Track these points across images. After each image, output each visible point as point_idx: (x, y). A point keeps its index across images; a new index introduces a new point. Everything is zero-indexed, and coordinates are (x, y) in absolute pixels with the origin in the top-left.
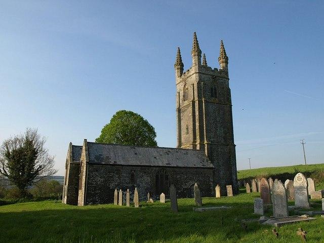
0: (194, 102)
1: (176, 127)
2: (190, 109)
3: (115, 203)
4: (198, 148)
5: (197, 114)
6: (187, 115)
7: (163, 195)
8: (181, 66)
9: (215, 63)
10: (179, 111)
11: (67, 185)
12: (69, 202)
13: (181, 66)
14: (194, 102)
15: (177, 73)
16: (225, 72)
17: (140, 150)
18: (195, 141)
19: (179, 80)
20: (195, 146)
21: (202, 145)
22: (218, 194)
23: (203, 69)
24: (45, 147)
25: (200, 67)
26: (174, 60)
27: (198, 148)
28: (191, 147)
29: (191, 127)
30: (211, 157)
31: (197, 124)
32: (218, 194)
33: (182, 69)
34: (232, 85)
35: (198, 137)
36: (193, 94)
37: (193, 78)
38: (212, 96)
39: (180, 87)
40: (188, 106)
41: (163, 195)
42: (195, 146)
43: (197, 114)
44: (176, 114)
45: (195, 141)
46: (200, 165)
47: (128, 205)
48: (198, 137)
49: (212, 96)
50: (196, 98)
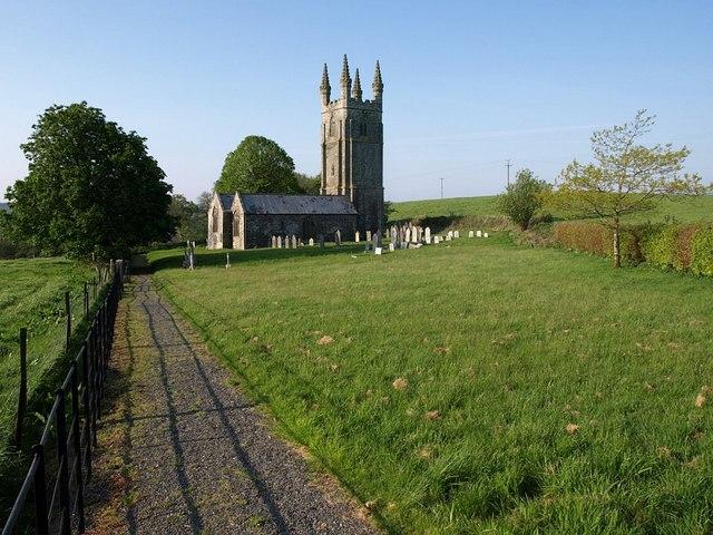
0: (340, 142)
1: (321, 165)
2: (337, 146)
3: (274, 247)
4: (343, 193)
5: (344, 155)
6: (333, 153)
7: (311, 240)
8: (327, 89)
9: (369, 95)
10: (324, 146)
11: (221, 230)
12: (361, 239)
13: (327, 89)
14: (340, 142)
15: (321, 98)
16: (378, 103)
17: (287, 198)
18: (340, 185)
19: (325, 109)
20: (340, 190)
21: (348, 190)
22: (357, 239)
23: (354, 104)
24: (26, 134)
25: (350, 100)
26: (319, 81)
27: (343, 193)
28: (335, 192)
29: (337, 171)
30: (356, 203)
31: (344, 167)
32: (357, 239)
33: (328, 94)
34: (388, 119)
35: (344, 181)
36: (340, 131)
37: (342, 113)
38: (361, 134)
39: (327, 117)
40: (334, 144)
41: (311, 240)
42: (340, 190)
43: (344, 155)
44: (321, 148)
45: (340, 185)
46: (344, 212)
47: (287, 247)
48: (344, 181)
49: (361, 134)
50: (343, 138)
